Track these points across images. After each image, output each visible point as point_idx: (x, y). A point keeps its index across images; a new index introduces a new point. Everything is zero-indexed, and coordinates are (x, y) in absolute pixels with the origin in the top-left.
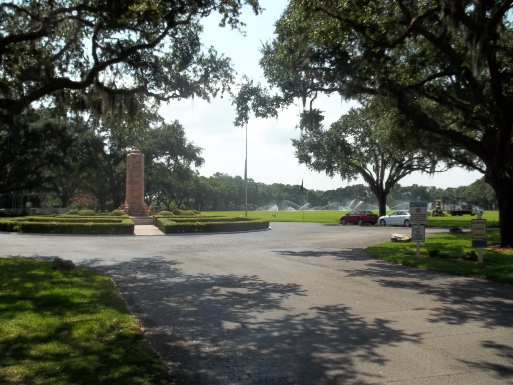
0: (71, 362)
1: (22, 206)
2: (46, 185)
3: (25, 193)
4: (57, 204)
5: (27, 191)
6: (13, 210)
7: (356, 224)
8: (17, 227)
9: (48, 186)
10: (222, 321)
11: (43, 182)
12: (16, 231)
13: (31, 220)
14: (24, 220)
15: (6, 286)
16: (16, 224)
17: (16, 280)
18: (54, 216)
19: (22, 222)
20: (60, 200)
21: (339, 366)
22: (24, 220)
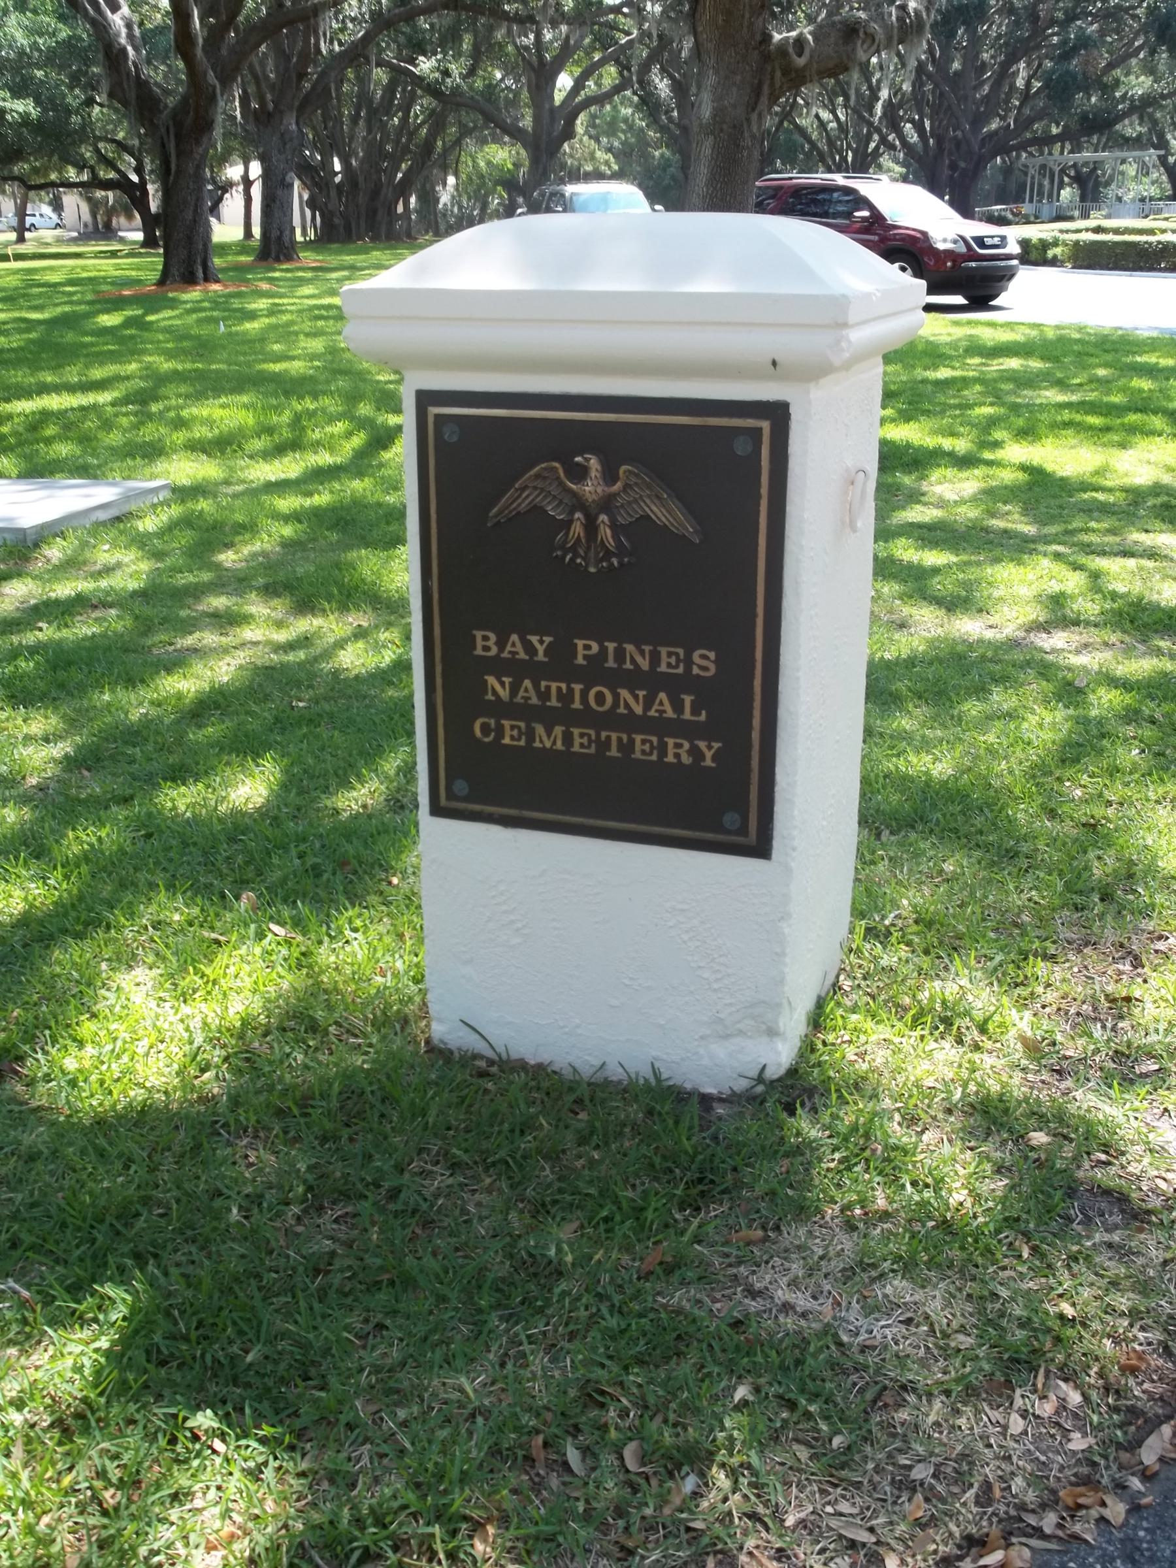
0: (279, 624)
1: (336, 221)
2: (1131, 128)
3: (1063, 156)
4: (1154, 191)
5: (1068, 146)
6: (1026, 208)
7: (1151, 268)
8: (1058, 251)
9: (1129, 132)
10: (353, 555)
11: (1119, 118)
12: (1054, 262)
13: (1098, 230)
14: (1078, 231)
15: (1080, 385)
16: (1056, 243)
17: (1101, 372)
18: (84, 269)
19: (1075, 237)
20: (1164, 178)
21: (1083, 560)
22: (1078, 231)
